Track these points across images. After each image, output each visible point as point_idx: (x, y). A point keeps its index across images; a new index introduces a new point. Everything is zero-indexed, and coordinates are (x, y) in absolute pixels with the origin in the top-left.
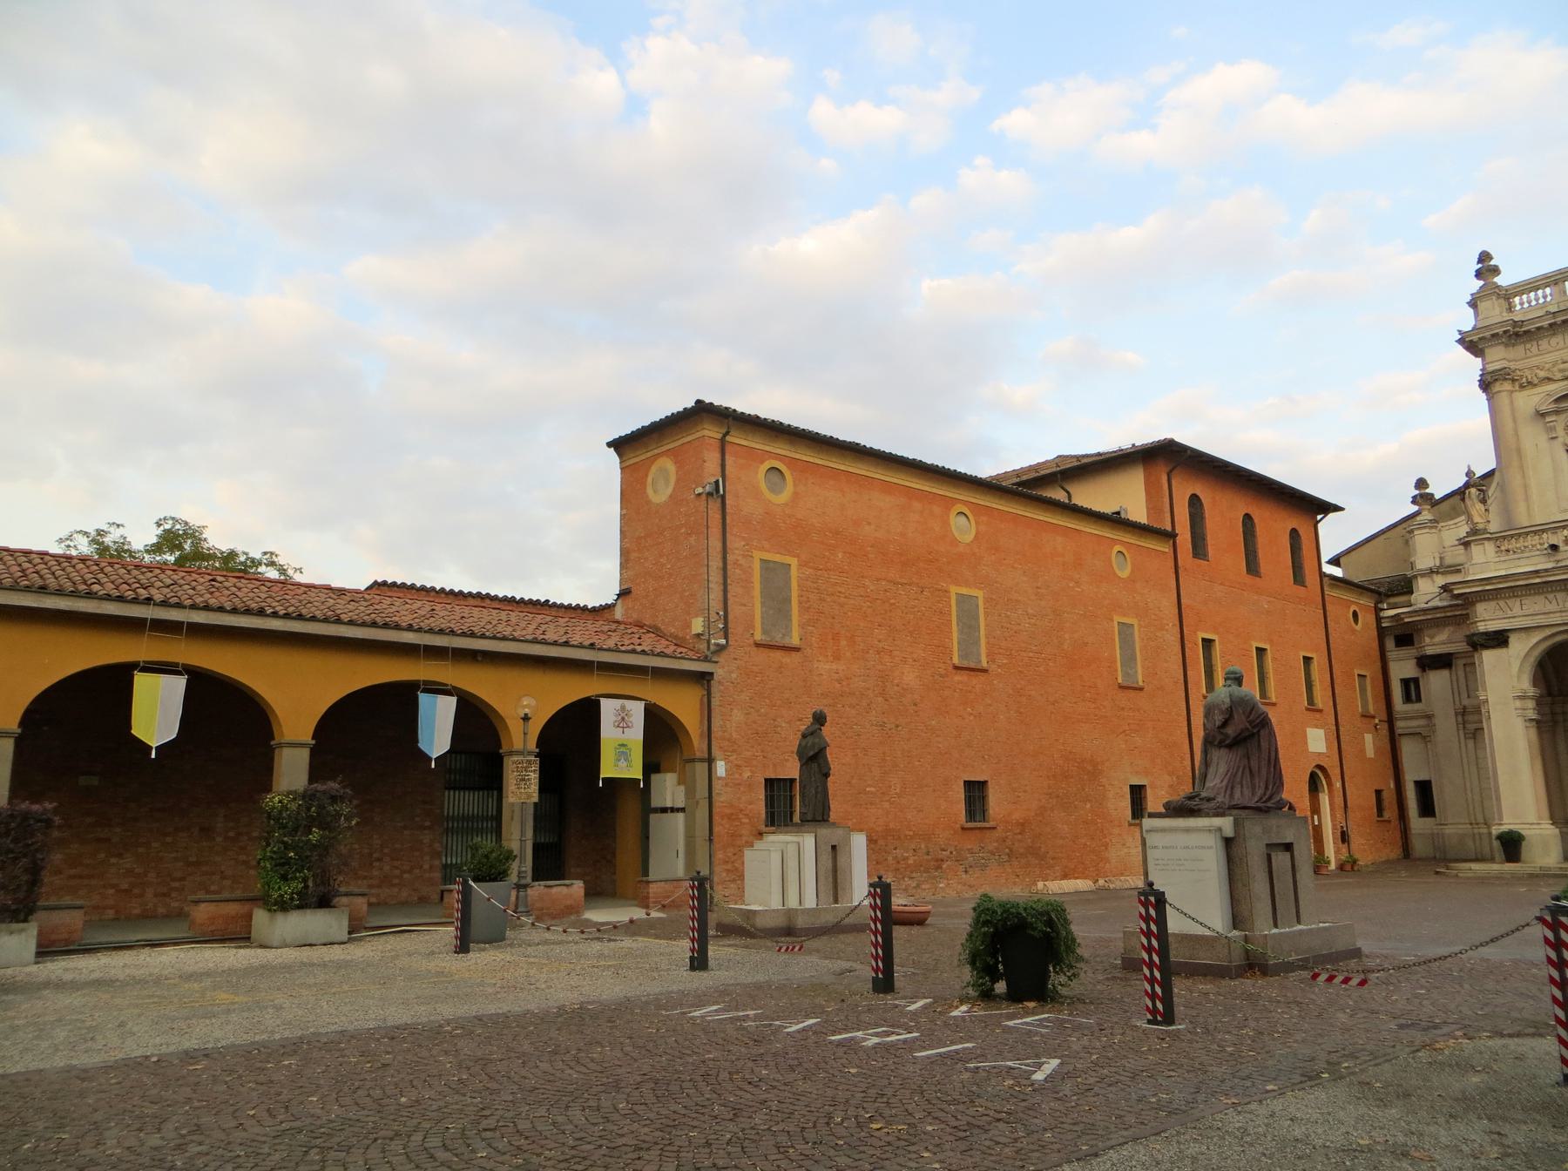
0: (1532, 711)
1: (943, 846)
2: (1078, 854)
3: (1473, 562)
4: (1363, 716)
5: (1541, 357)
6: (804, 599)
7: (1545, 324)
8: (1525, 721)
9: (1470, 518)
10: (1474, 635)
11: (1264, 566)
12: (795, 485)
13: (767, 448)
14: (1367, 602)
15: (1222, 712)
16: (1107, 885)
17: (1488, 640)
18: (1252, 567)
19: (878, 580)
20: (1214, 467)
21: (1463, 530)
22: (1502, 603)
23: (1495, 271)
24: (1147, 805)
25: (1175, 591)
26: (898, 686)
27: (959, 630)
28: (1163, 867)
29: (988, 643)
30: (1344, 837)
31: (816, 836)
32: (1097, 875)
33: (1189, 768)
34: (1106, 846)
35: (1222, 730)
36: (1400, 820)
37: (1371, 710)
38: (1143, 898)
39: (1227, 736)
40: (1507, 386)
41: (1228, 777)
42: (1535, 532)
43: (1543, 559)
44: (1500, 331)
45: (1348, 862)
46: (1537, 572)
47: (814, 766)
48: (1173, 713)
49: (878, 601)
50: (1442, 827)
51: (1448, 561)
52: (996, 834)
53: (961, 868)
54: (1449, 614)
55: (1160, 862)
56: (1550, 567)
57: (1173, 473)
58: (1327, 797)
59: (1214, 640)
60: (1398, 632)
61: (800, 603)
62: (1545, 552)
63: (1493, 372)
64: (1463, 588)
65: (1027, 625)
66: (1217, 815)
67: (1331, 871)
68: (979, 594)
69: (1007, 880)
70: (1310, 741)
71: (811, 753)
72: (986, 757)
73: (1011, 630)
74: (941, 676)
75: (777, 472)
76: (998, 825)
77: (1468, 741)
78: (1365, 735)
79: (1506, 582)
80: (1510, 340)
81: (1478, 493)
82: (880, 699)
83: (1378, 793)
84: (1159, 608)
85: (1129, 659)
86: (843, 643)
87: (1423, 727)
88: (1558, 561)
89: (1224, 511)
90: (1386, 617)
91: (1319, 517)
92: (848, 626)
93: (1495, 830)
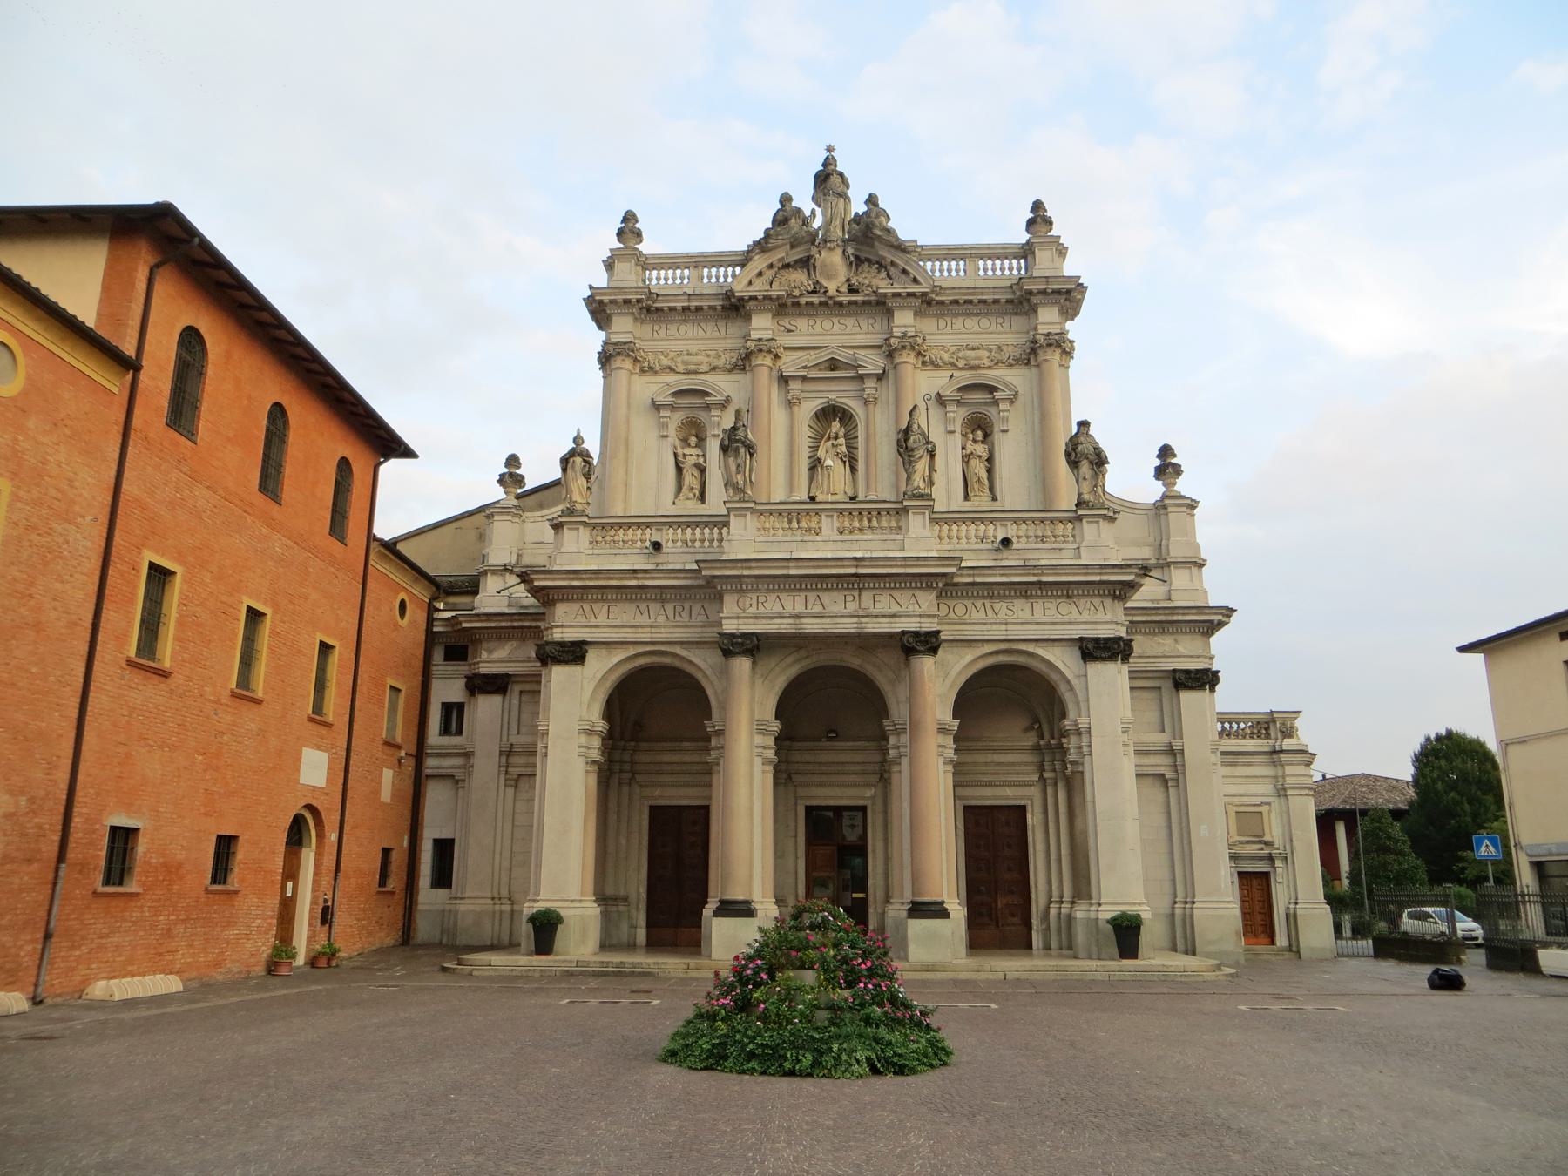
0: (596, 751)
3: (563, 550)
4: (387, 743)
5: (668, 343)
7: (679, 305)
8: (587, 763)
10: (547, 643)
14: (422, 593)
17: (562, 652)
18: (270, 481)
22: (586, 607)
23: (638, 235)
25: (114, 467)
33: (63, 786)
36: (406, 890)
37: (399, 740)
40: (628, 364)
42: (639, 525)
43: (641, 559)
44: (634, 297)
45: (324, 954)
46: (635, 571)
48: (52, 678)
50: (458, 902)
54: (516, 624)
57: (161, 270)
58: (312, 855)
60: (451, 641)
62: (646, 551)
67: (298, 967)
70: (304, 769)
78: (385, 770)
79: (596, 579)
80: (640, 314)
81: (583, 464)
83: (386, 852)
84: (71, 481)
87: (459, 768)
88: (659, 564)
93: (529, 909)
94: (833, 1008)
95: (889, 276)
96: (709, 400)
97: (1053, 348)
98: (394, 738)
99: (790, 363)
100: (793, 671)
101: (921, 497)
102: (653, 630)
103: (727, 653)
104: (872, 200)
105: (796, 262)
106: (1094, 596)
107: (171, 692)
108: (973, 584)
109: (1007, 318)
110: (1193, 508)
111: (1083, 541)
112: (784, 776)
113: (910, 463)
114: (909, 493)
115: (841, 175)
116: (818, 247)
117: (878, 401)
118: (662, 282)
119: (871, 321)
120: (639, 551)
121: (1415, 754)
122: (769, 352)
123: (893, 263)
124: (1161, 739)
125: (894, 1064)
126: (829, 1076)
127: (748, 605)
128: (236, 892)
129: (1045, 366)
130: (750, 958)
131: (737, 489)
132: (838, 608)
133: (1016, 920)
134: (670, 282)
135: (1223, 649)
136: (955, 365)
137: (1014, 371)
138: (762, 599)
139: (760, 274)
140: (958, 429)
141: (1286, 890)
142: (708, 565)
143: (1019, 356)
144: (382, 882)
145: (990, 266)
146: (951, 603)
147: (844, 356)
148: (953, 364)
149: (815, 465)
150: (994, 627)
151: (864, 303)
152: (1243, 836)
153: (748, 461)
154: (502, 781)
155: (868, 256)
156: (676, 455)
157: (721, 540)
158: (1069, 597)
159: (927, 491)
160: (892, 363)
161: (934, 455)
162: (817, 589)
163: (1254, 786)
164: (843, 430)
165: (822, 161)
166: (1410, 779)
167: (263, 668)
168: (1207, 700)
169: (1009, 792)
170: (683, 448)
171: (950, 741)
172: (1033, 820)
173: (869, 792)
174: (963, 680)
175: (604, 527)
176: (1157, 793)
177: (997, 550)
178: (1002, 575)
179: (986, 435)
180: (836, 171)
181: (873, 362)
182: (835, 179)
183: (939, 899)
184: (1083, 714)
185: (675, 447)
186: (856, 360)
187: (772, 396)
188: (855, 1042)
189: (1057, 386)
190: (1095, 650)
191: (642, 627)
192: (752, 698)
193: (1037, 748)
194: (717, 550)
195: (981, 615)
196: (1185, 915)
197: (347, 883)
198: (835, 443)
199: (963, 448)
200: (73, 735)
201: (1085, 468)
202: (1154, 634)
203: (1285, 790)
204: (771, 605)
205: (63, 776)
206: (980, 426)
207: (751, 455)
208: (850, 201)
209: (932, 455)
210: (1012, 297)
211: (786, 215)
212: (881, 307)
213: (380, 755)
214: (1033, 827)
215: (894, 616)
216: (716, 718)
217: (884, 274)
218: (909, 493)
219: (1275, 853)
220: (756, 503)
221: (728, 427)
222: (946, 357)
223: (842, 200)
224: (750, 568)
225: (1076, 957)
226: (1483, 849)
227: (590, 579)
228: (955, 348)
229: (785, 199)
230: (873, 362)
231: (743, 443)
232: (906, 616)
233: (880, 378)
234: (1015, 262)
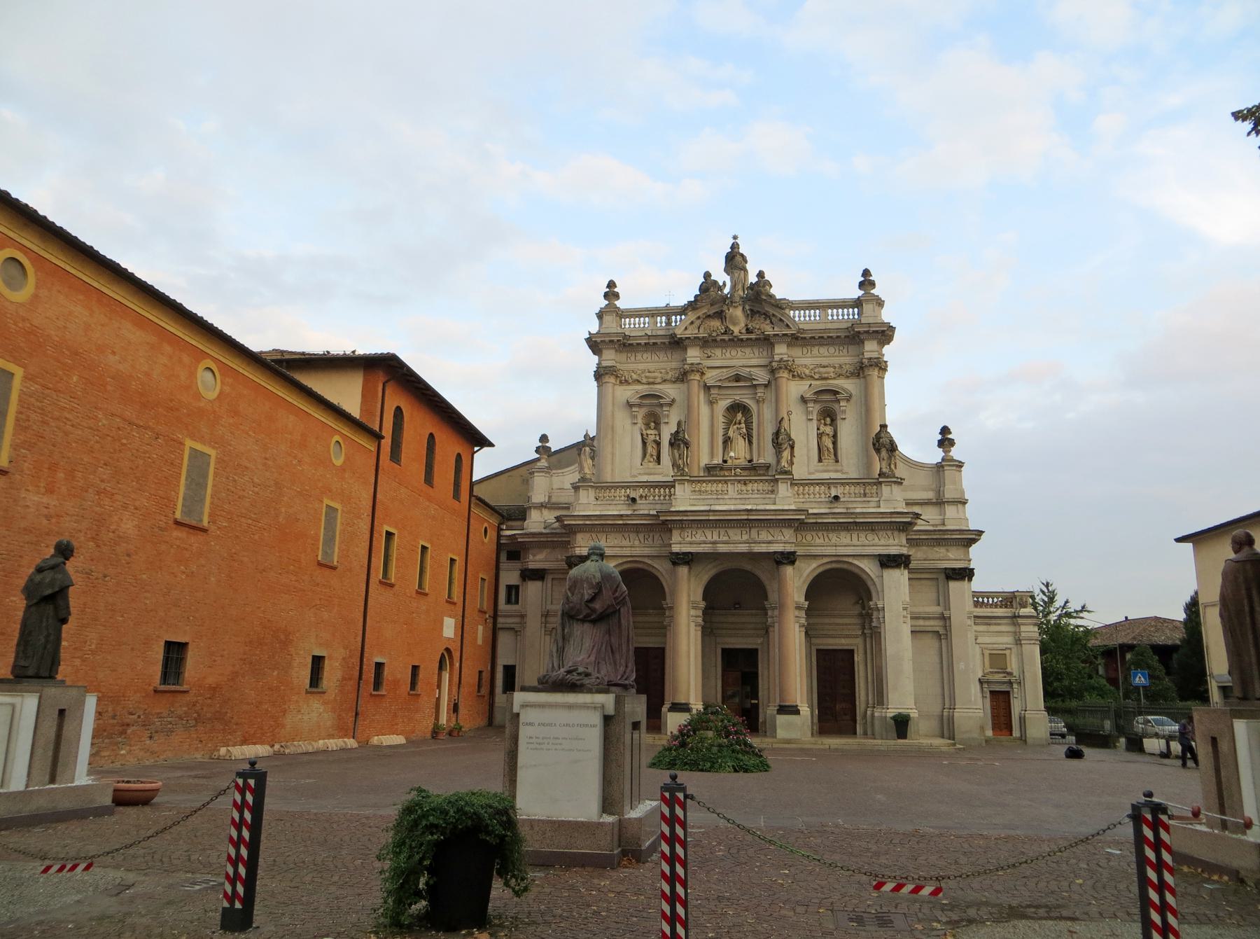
1: (131, 710)
2: (259, 720)
3: (580, 502)
6: (23, 417)
7: (643, 342)
9: (581, 469)
10: (572, 557)
11: (437, 479)
12: (37, 287)
13: (11, 234)
14: (494, 521)
15: (591, 586)
16: (282, 750)
18: (429, 479)
19: (113, 415)
20: (417, 388)
21: (575, 477)
22: (594, 535)
23: (617, 296)
24: (323, 674)
26: (113, 532)
27: (186, 484)
28: (538, 746)
29: (212, 503)
30: (455, 708)
31: (40, 697)
32: (272, 740)
34: (284, 712)
35: (590, 605)
37: (485, 608)
38: (667, 795)
39: (594, 610)
40: (612, 380)
41: (595, 650)
43: (625, 507)
44: (616, 339)
46: (622, 515)
47: (49, 609)
49: (109, 438)
51: (554, 500)
52: (187, 698)
53: (147, 734)
54: (549, 539)
55: (533, 740)
56: (629, 513)
58: (448, 675)
59: (394, 534)
61: (17, 420)
63: (606, 367)
64: (572, 520)
65: (251, 493)
66: (599, 692)
68: (213, 453)
69: (190, 745)
71: (49, 592)
72: (191, 618)
73: (236, 494)
74: (161, 529)
75: (17, 264)
76: (191, 689)
77: (546, 637)
80: (619, 348)
82: (91, 544)
83: (480, 672)
85: (330, 540)
86: (61, 475)
89: (418, 425)
90: (504, 536)
91: (476, 449)
92: (69, 458)
94: (720, 746)
95: (771, 322)
96: (662, 401)
97: (873, 367)
98: (483, 608)
99: (711, 377)
100: (713, 572)
101: (786, 473)
102: (633, 549)
103: (674, 564)
104: (761, 275)
105: (714, 313)
106: (887, 530)
107: (394, 594)
108: (816, 523)
109: (846, 347)
110: (961, 467)
111: (882, 496)
112: (709, 630)
113: (780, 452)
114: (779, 471)
115: (742, 255)
116: (727, 305)
117: (766, 402)
118: (632, 326)
119: (761, 350)
120: (623, 502)
121: (1186, 604)
122: (698, 371)
123: (774, 315)
124: (937, 610)
125: (744, 768)
126: (717, 772)
127: (686, 536)
128: (420, 695)
129: (868, 378)
130: (686, 726)
131: (678, 467)
132: (738, 538)
133: (848, 717)
134: (637, 326)
135: (977, 556)
136: (813, 377)
137: (849, 381)
138: (694, 533)
139: (692, 323)
140: (815, 417)
141: (1020, 702)
142: (663, 514)
143: (852, 371)
144: (479, 691)
145: (835, 313)
146: (804, 534)
147: (744, 372)
148: (812, 377)
149: (727, 441)
150: (829, 548)
151: (756, 339)
152: (994, 669)
153: (685, 452)
154: (543, 632)
155: (759, 310)
156: (642, 435)
157: (670, 496)
158: (873, 530)
159: (790, 469)
160: (774, 377)
161: (793, 447)
162: (725, 527)
163: (1000, 638)
164: (744, 418)
165: (730, 246)
166: (1182, 620)
167: (428, 577)
168: (966, 587)
169: (843, 641)
170: (646, 430)
171: (803, 614)
172: (858, 658)
173: (759, 641)
174: (811, 578)
175: (603, 487)
176: (931, 644)
177: (831, 502)
178: (832, 518)
179: (833, 420)
180: (739, 253)
181: (762, 376)
182: (738, 258)
183: (795, 704)
184: (881, 599)
185: (642, 430)
186: (751, 375)
187: (700, 399)
188: (727, 759)
189: (876, 391)
190: (889, 562)
191: (626, 547)
192: (689, 588)
193: (861, 615)
194: (668, 502)
195: (821, 541)
196: (949, 715)
197: (464, 690)
198: (739, 426)
199: (818, 429)
200: (362, 620)
201: (884, 453)
202: (934, 546)
203: (1020, 640)
204: (699, 537)
205: (359, 639)
206: (829, 416)
207: (687, 448)
208: (747, 272)
209: (792, 447)
210: (848, 334)
211: (708, 285)
212: (766, 342)
213: (477, 618)
214: (858, 662)
215: (769, 542)
216: (668, 600)
217: (768, 321)
218: (779, 471)
219: (1013, 679)
220: (690, 477)
221: (673, 432)
222: (807, 372)
223: (743, 272)
224: (687, 516)
225: (875, 739)
226: (1137, 679)
227: (596, 520)
228: (812, 366)
229: (707, 275)
230: (762, 376)
231: (683, 441)
232: (776, 543)
233: (766, 386)
234: (851, 310)
